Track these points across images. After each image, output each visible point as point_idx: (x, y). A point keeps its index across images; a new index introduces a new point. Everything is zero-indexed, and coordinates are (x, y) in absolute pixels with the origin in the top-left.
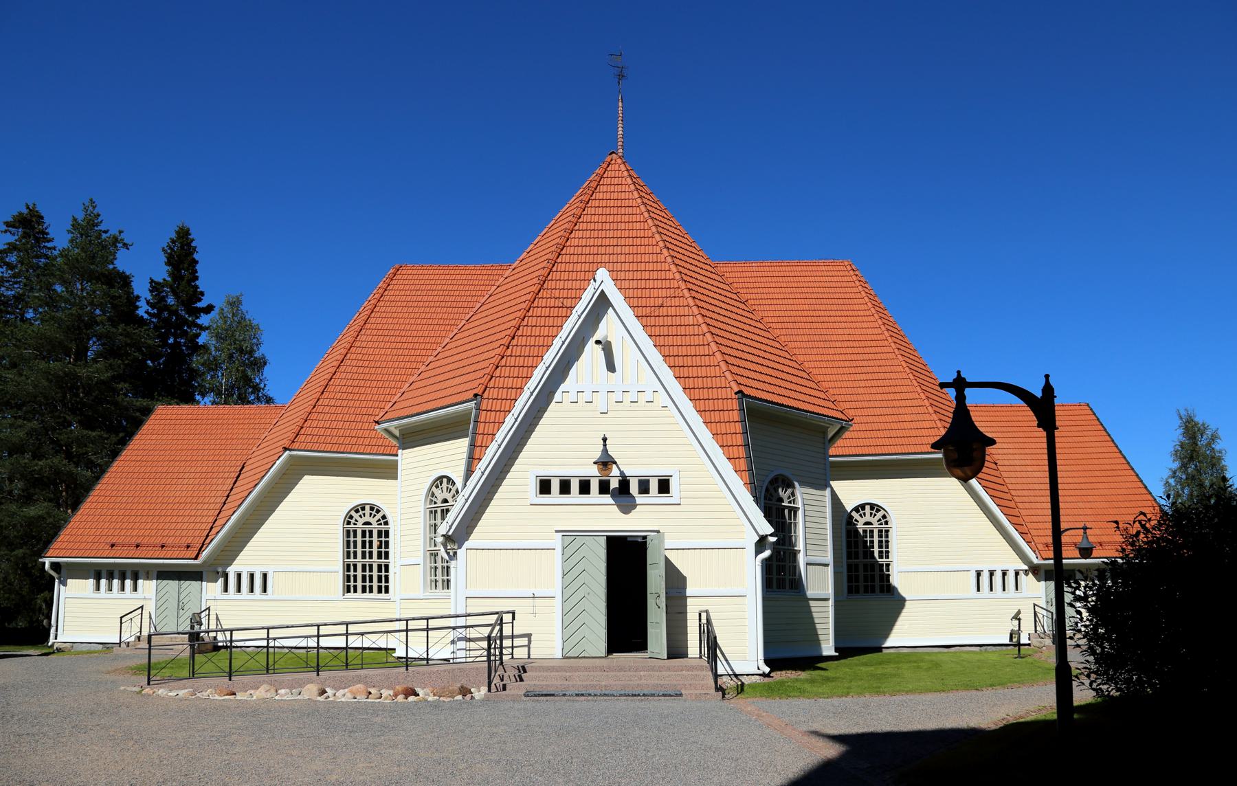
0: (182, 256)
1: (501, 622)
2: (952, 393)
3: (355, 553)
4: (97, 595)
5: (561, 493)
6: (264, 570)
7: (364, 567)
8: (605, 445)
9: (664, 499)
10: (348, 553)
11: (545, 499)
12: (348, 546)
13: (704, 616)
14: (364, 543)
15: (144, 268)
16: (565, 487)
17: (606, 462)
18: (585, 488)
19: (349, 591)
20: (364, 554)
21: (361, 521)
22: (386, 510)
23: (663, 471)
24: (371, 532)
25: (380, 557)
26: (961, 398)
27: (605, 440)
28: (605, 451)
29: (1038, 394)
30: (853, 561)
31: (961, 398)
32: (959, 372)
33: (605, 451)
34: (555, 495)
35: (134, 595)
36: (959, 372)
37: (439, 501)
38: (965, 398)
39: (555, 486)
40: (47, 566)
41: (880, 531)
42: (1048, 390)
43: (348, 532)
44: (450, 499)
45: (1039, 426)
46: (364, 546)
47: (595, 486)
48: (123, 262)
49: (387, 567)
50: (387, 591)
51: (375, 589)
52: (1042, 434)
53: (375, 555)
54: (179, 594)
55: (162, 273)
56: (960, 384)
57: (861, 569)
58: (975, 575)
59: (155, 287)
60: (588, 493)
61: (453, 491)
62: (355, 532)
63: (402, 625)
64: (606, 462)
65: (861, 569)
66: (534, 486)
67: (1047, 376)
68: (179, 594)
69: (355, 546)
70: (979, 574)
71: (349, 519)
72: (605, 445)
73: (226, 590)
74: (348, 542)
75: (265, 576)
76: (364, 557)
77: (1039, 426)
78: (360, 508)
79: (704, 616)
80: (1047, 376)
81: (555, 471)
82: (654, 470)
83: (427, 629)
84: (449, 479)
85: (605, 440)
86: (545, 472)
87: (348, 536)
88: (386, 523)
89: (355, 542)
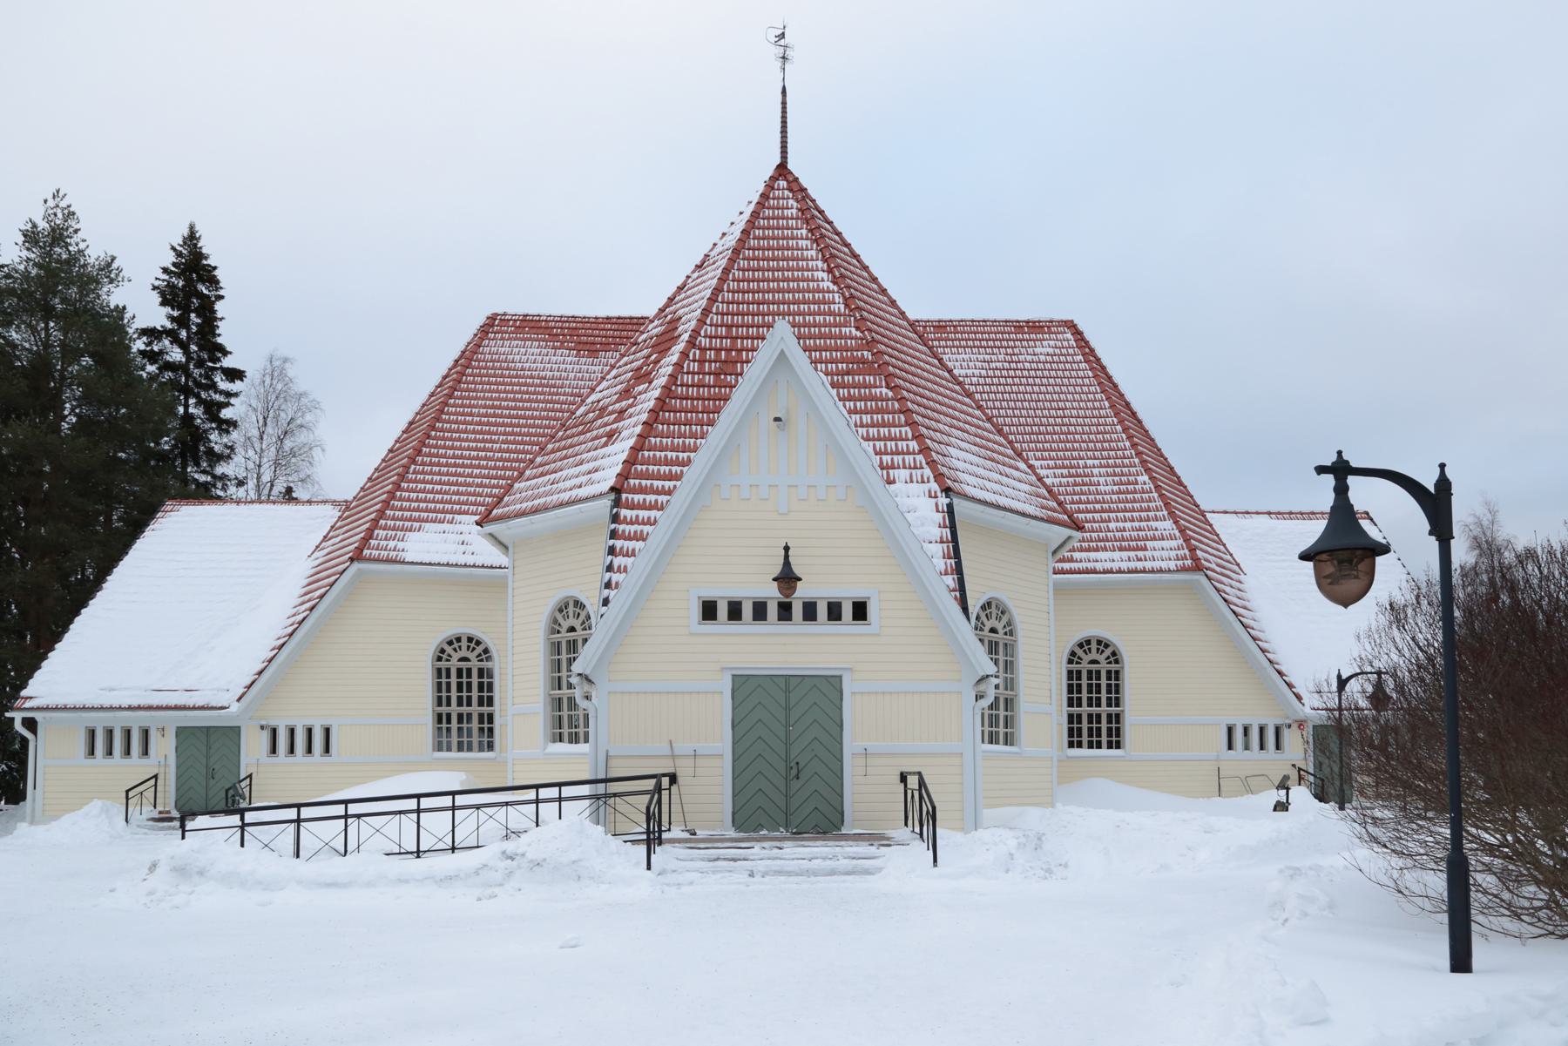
0: (192, 282)
1: (658, 789)
2: (1329, 480)
3: (449, 699)
4: (91, 761)
5: (755, 619)
6: (326, 723)
7: (460, 716)
8: (787, 556)
9: (859, 628)
10: (440, 698)
11: (709, 627)
12: (440, 690)
13: (913, 782)
14: (460, 686)
15: (140, 304)
16: (735, 612)
17: (787, 578)
18: (760, 611)
19: (440, 749)
20: (460, 699)
21: (456, 656)
22: (488, 641)
23: (859, 594)
24: (469, 671)
25: (481, 704)
26: (1341, 490)
27: (787, 549)
28: (787, 563)
29: (1429, 483)
30: (1075, 710)
31: (1341, 490)
32: (1340, 453)
33: (787, 563)
34: (722, 627)
35: (145, 761)
36: (1340, 453)
37: (987, 629)
38: (1347, 488)
39: (723, 610)
40: (18, 726)
41: (1109, 672)
42: (1444, 484)
43: (439, 671)
44: (578, 627)
45: (1431, 533)
46: (460, 689)
47: (772, 610)
48: (115, 297)
49: (1070, 704)
50: (491, 747)
51: (1104, 744)
52: (1433, 544)
53: (475, 701)
54: (208, 757)
55: (159, 317)
56: (1341, 470)
57: (1085, 719)
58: (1225, 731)
59: (151, 333)
60: (839, 618)
61: (582, 617)
62: (448, 670)
63: (411, 804)
64: (787, 578)
65: (1085, 719)
66: (696, 611)
67: (1442, 466)
68: (208, 757)
69: (449, 690)
70: (1230, 730)
71: (1073, 657)
72: (787, 556)
73: (274, 750)
74: (439, 684)
75: (327, 731)
76: (460, 704)
77: (1431, 533)
78: (1084, 644)
79: (913, 782)
80: (1442, 466)
81: (722, 592)
82: (847, 592)
83: (418, 811)
84: (577, 603)
85: (787, 549)
86: (710, 594)
87: (440, 676)
88: (443, 651)
89: (449, 684)
